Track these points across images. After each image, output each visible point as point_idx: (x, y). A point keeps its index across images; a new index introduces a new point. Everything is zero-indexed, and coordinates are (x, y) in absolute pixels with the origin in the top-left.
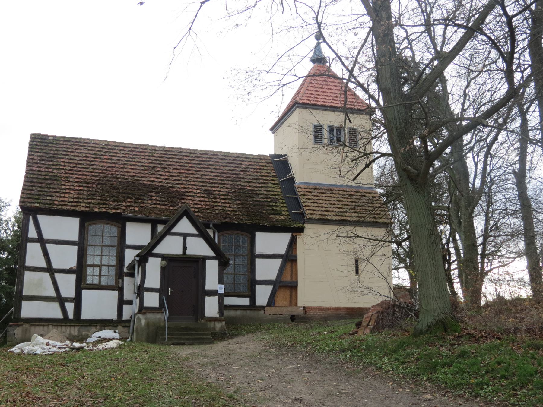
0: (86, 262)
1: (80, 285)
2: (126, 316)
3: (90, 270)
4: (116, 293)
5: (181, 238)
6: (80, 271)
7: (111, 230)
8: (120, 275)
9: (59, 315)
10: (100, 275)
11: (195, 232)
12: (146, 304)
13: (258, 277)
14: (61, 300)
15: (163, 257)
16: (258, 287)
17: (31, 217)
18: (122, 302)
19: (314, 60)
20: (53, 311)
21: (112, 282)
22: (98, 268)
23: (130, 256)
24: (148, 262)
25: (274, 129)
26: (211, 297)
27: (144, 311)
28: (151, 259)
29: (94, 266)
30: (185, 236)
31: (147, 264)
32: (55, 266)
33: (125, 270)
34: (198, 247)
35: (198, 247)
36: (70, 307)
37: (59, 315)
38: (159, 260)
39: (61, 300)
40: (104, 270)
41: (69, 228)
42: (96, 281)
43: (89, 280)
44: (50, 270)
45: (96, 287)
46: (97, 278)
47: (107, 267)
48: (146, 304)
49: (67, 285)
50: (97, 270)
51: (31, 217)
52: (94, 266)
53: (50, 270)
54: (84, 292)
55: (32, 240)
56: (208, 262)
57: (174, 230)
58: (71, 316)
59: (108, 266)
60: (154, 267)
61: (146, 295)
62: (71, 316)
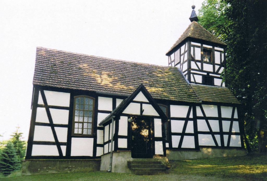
0: (74, 120)
1: (71, 135)
2: (98, 154)
3: (76, 125)
4: (92, 140)
5: (37, 127)
6: (70, 126)
7: (89, 102)
8: (95, 128)
9: (57, 154)
10: (83, 128)
11: (147, 101)
12: (120, 146)
13: (173, 131)
14: (58, 144)
15: (129, 116)
16: (173, 137)
17: (40, 91)
18: (96, 145)
19: (192, 20)
20: (52, 151)
21: (90, 132)
22: (82, 124)
23: (101, 117)
24: (120, 119)
25: (169, 54)
26: (158, 142)
27: (118, 151)
28: (122, 117)
29: (79, 122)
30: (141, 103)
31: (119, 120)
32: (55, 122)
33: (98, 126)
34: (150, 110)
35: (150, 110)
36: (64, 148)
37: (57, 154)
38: (126, 118)
39: (58, 144)
40: (85, 125)
41: (64, 99)
42: (80, 132)
43: (76, 132)
44: (52, 125)
45: (81, 136)
46: (81, 130)
47: (86, 124)
48: (120, 146)
49: (62, 135)
50: (81, 125)
51: (40, 91)
52: (79, 122)
53: (52, 125)
54: (73, 139)
55: (41, 106)
56: (156, 120)
57: (134, 100)
58: (64, 154)
59: (88, 123)
60: (123, 122)
61: (120, 140)
62: (64, 154)
